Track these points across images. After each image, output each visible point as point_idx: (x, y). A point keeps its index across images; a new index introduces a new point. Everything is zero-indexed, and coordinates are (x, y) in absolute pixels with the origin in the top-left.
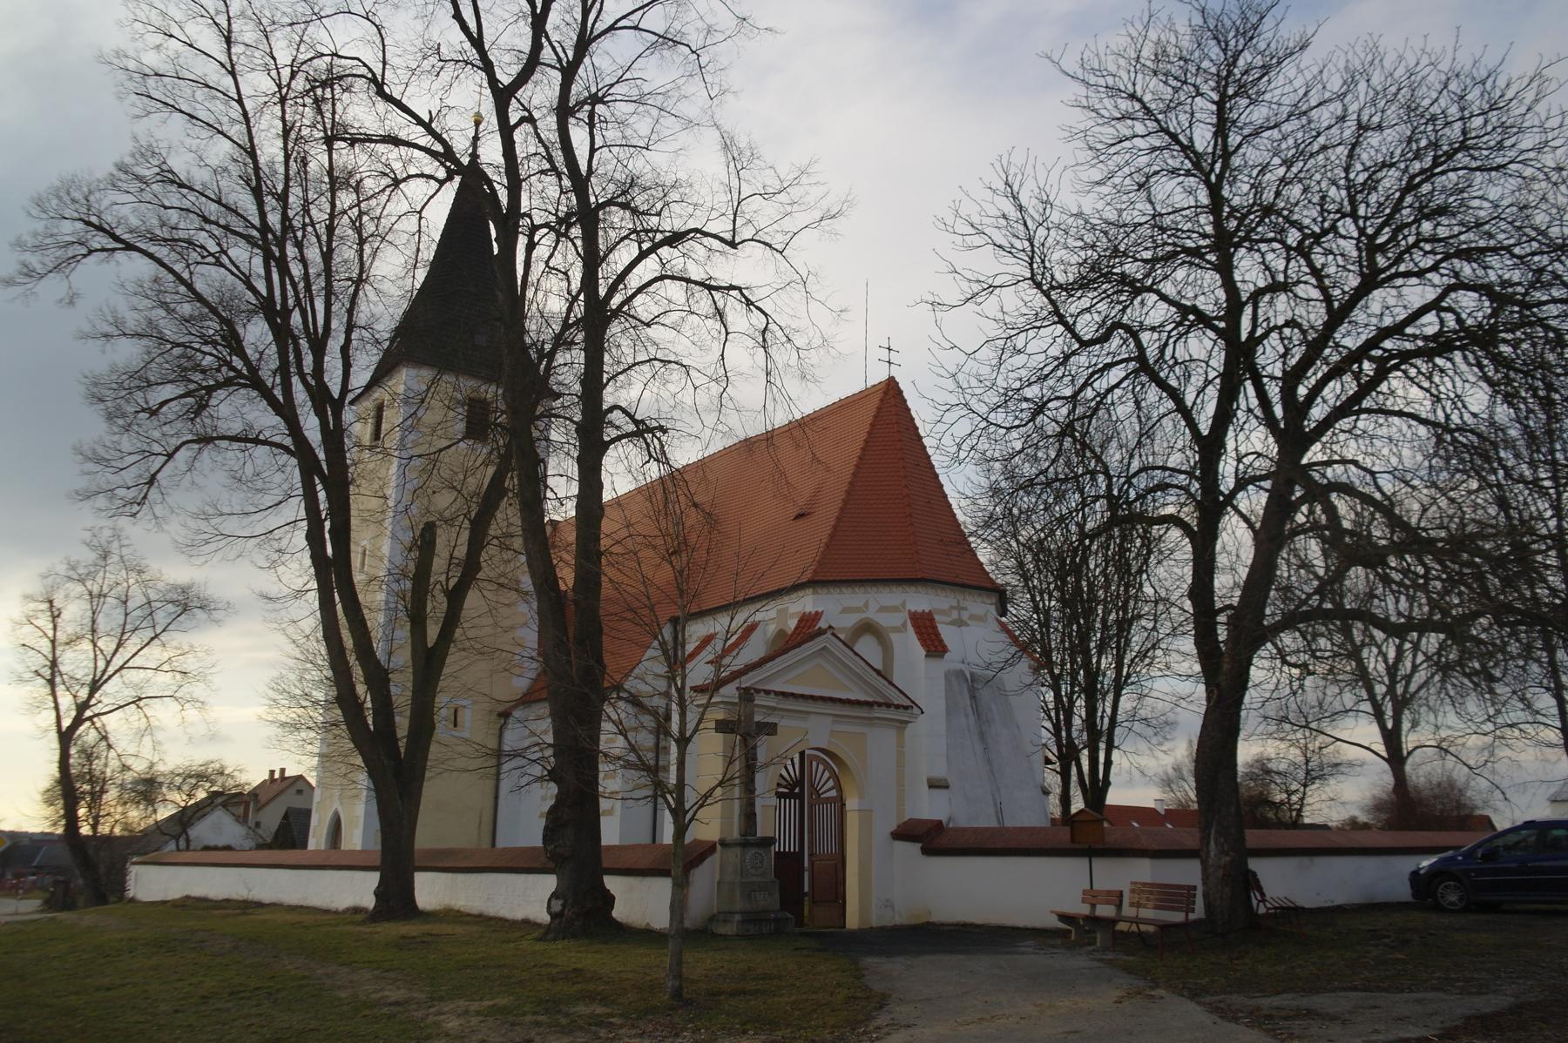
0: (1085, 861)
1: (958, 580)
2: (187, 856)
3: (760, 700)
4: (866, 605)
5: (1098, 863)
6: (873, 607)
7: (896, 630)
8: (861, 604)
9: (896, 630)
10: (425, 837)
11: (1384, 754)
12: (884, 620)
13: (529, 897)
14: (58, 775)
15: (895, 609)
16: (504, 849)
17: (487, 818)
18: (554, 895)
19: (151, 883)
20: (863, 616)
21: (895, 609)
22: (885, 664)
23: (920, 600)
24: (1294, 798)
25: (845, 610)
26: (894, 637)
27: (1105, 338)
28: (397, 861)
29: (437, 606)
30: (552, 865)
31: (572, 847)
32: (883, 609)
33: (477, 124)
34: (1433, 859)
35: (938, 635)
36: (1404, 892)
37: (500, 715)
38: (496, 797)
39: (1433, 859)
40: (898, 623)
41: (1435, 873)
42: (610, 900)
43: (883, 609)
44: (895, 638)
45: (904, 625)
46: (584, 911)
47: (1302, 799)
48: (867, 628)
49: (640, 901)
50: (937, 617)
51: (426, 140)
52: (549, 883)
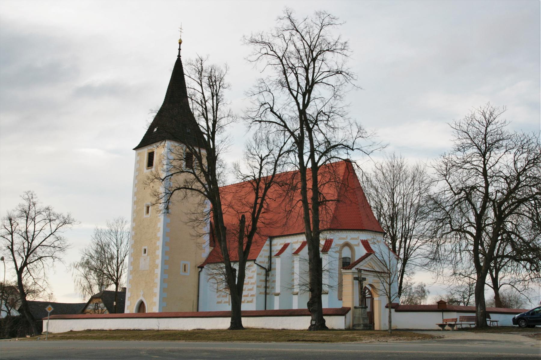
0: (441, 313)
1: (374, 230)
2: (102, 315)
3: (363, 272)
4: (347, 237)
5: (445, 314)
6: (349, 238)
7: (356, 245)
8: (345, 237)
9: (356, 245)
10: (244, 307)
11: (492, 286)
12: (352, 242)
13: (303, 323)
14: (494, 295)
15: (356, 239)
16: (269, 311)
17: (195, 303)
18: (312, 320)
19: (53, 326)
20: (345, 241)
21: (356, 239)
22: (352, 255)
23: (364, 236)
24: (466, 300)
25: (340, 239)
26: (356, 248)
27: (460, 193)
28: (236, 315)
29: (245, 240)
30: (310, 313)
31: (315, 308)
32: (352, 239)
33: (180, 43)
34: (519, 315)
35: (370, 247)
36: (511, 323)
37: (199, 267)
38: (198, 296)
39: (519, 315)
40: (357, 243)
41: (519, 318)
42: (324, 321)
43: (352, 239)
44: (356, 248)
45: (359, 244)
46: (319, 325)
47: (468, 300)
48: (347, 244)
49: (332, 322)
50: (369, 242)
51: (279, 121)
52: (310, 318)
